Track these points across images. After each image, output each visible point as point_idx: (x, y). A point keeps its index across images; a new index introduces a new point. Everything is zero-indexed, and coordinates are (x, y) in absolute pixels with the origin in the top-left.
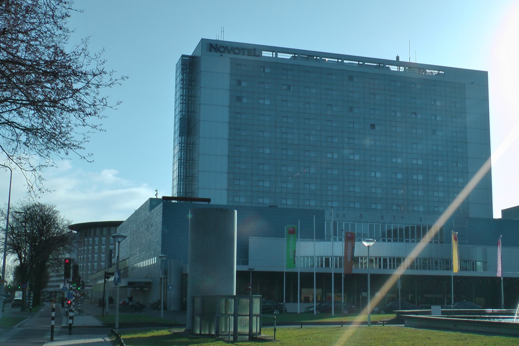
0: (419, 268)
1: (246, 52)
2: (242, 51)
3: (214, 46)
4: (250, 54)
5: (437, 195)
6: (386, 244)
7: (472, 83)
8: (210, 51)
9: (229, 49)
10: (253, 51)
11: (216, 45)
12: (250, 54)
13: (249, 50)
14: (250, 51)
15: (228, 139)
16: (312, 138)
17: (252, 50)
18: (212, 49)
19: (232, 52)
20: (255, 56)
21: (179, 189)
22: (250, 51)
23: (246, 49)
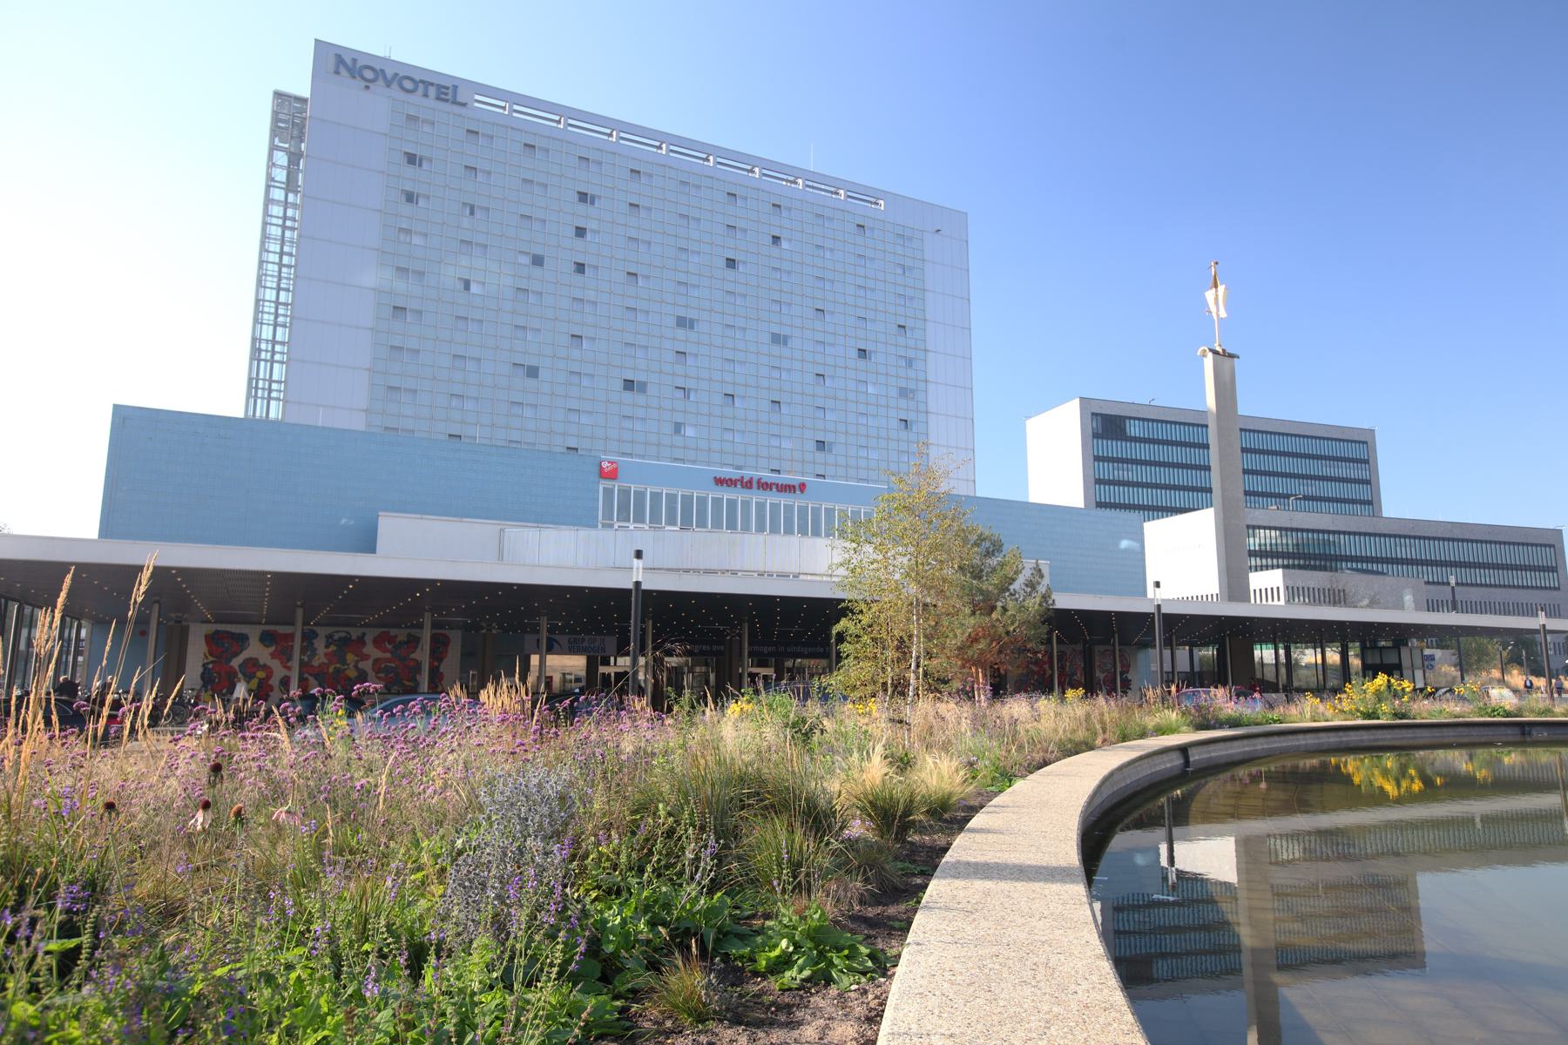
0: (1321, 833)
1: (432, 91)
2: (421, 86)
3: (349, 62)
4: (443, 96)
5: (731, 439)
6: (450, 654)
7: (938, 231)
8: (337, 72)
9: (389, 76)
10: (450, 92)
11: (354, 61)
12: (443, 96)
13: (439, 87)
14: (443, 90)
15: (368, 369)
16: (871, 390)
17: (447, 88)
18: (343, 71)
19: (395, 86)
20: (455, 102)
21: (1078, 883)
22: (443, 90)
23: (432, 84)
